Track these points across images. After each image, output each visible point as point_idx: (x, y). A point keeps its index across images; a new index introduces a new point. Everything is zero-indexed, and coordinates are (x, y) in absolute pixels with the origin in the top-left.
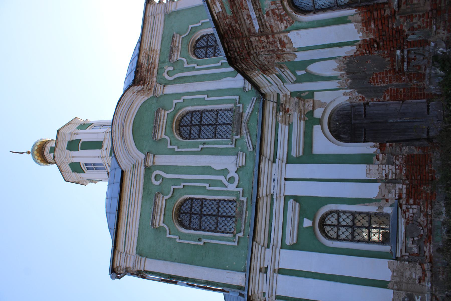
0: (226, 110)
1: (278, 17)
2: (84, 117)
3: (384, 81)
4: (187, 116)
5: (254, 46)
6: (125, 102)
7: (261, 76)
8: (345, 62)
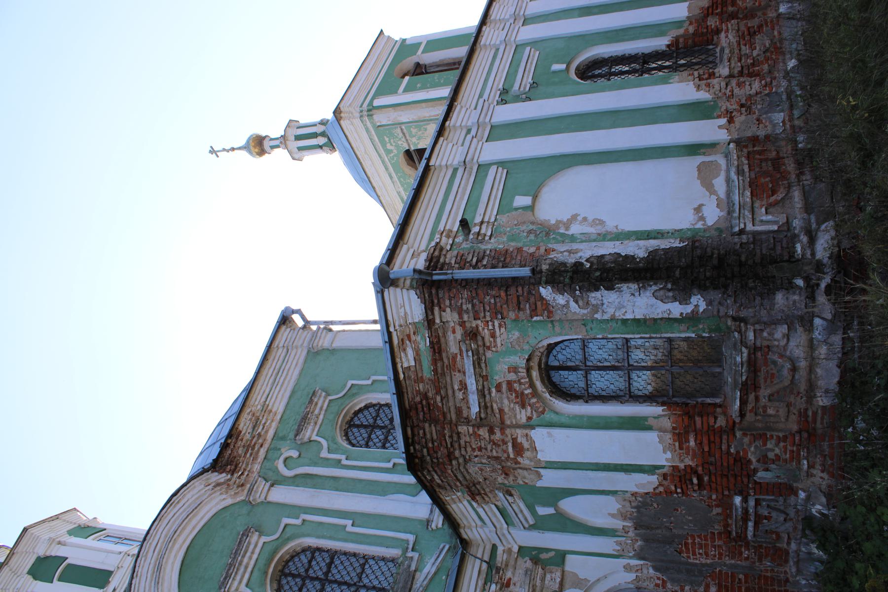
0: (383, 559)
1: (517, 397)
2: (89, 512)
3: (707, 554)
4: (303, 557)
5: (462, 443)
6: (185, 500)
7: (465, 503)
8: (634, 504)
